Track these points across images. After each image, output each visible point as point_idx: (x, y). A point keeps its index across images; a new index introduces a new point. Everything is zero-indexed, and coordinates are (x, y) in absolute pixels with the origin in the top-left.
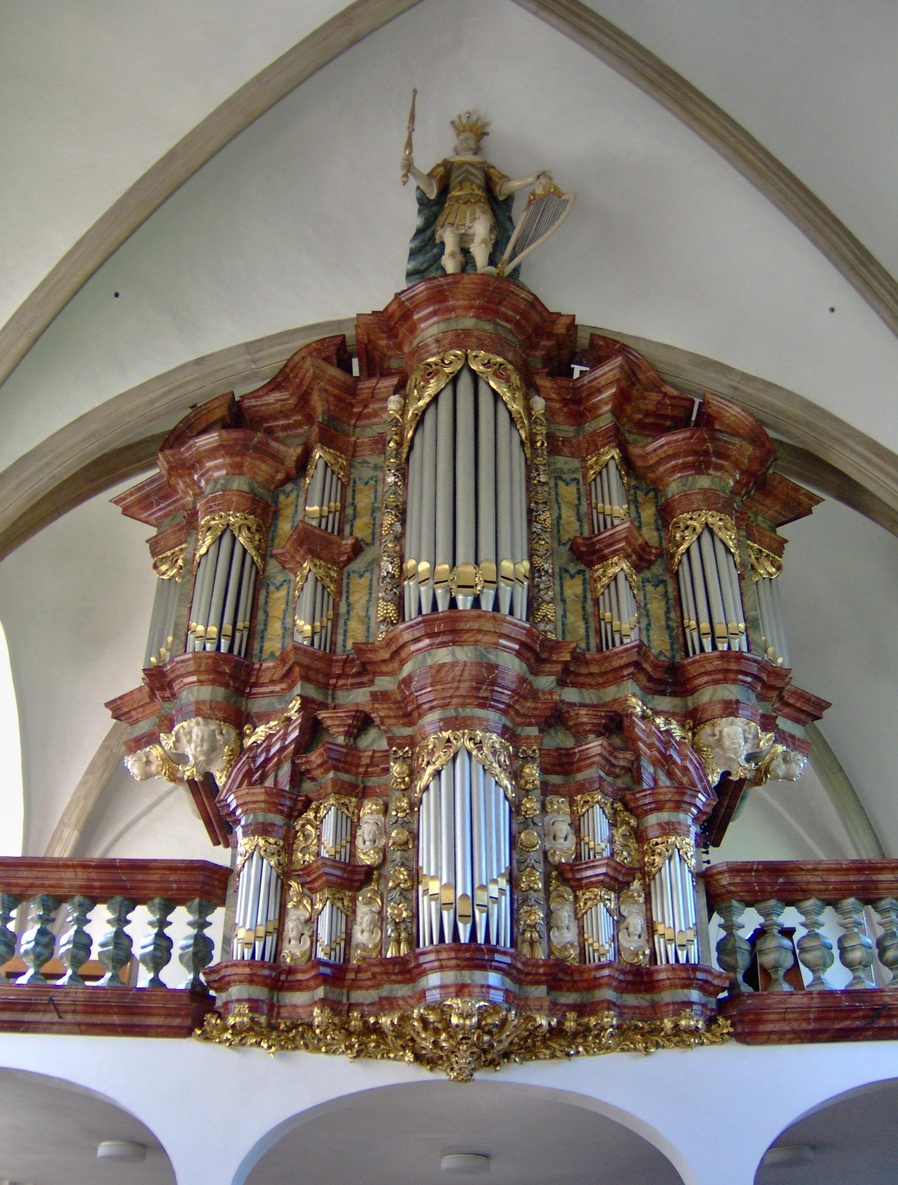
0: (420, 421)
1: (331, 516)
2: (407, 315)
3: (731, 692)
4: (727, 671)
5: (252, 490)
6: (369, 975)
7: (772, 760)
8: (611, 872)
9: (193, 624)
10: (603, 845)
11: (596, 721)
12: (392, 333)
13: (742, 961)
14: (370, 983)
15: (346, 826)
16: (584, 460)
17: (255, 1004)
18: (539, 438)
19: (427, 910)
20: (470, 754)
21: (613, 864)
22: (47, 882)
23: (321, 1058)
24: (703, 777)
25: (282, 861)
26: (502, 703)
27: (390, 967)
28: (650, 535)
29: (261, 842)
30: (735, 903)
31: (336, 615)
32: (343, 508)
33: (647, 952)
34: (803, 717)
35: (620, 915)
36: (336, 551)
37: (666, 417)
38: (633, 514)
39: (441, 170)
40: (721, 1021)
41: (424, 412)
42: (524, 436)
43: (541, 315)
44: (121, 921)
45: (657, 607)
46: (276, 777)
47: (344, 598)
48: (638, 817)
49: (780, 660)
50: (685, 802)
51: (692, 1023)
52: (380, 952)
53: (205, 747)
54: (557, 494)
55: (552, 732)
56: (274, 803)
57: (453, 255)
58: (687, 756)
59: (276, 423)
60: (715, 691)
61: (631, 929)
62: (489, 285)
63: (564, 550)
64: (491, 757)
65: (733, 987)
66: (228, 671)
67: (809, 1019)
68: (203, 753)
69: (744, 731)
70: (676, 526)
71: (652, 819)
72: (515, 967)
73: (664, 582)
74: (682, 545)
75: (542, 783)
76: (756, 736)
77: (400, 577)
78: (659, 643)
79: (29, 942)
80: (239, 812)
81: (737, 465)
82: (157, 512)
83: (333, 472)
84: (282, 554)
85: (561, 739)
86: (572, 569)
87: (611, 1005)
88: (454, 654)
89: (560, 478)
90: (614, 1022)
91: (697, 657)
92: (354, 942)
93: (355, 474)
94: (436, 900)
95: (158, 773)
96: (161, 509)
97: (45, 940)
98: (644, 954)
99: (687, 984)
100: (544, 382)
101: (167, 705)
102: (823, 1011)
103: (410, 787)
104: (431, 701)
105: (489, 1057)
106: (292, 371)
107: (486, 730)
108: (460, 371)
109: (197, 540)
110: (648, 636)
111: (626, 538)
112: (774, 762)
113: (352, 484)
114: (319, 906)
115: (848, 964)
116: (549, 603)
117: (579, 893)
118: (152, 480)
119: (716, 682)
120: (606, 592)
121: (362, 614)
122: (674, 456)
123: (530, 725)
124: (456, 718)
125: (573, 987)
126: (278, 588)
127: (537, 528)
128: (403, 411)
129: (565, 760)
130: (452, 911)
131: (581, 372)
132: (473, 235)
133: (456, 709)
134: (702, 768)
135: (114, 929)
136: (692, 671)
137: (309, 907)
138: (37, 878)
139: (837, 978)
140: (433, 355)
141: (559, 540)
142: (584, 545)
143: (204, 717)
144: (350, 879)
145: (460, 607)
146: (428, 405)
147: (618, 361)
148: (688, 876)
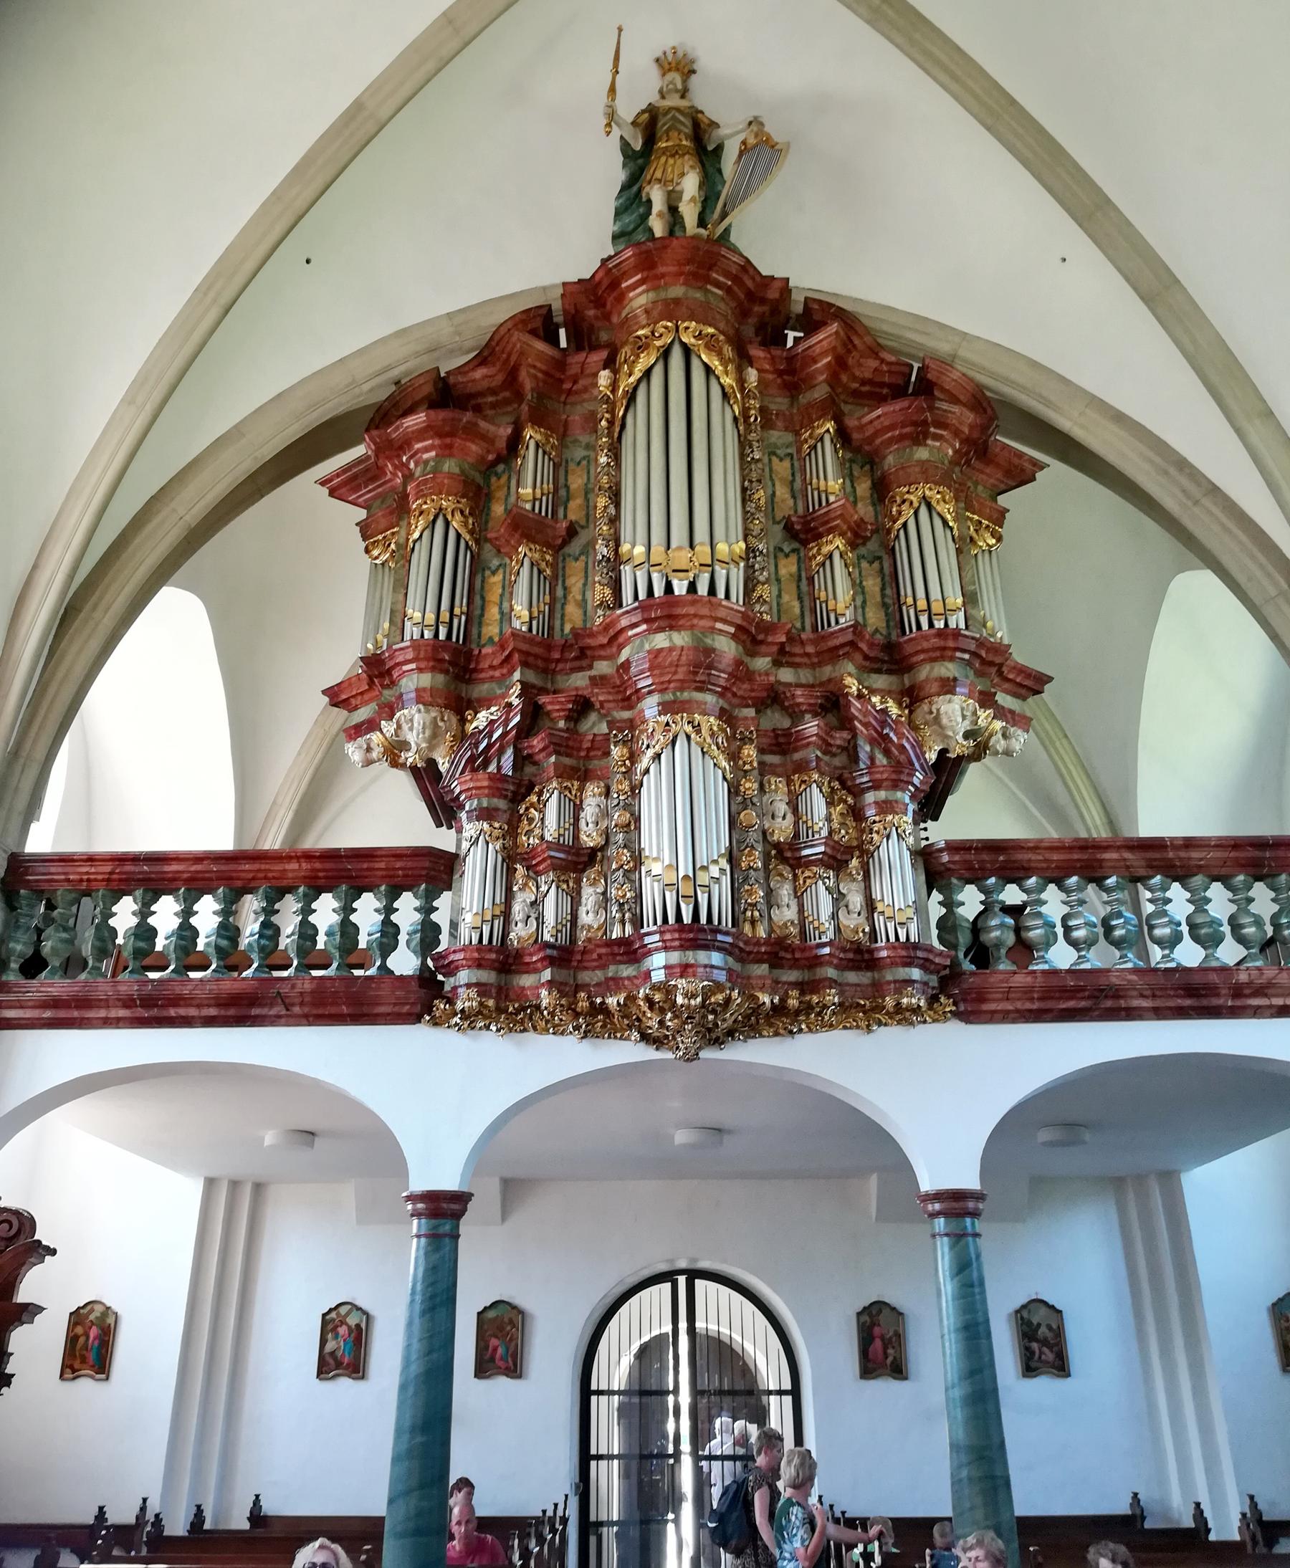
0: (631, 398)
1: (544, 498)
2: (614, 284)
3: (948, 669)
4: (944, 649)
5: (462, 471)
6: (595, 956)
7: (991, 736)
8: (829, 851)
9: (410, 611)
10: (821, 824)
11: (812, 701)
12: (599, 303)
13: (964, 939)
15: (569, 809)
16: (797, 434)
18: (753, 412)
19: (651, 892)
20: (688, 737)
22: (270, 875)
23: (549, 1039)
24: (921, 755)
28: (865, 510)
29: (486, 826)
30: (954, 881)
31: (553, 599)
33: (867, 930)
34: (1023, 691)
36: (555, 536)
37: (882, 385)
38: (849, 489)
41: (635, 389)
44: (347, 910)
45: (872, 584)
46: (499, 762)
47: (560, 582)
48: (855, 796)
51: (914, 1001)
52: (605, 933)
53: (428, 733)
54: (771, 470)
56: (498, 789)
57: (660, 215)
60: (932, 669)
61: (851, 907)
62: (698, 249)
63: (778, 528)
64: (709, 740)
65: (955, 964)
68: (425, 740)
69: (962, 709)
72: (737, 946)
73: (879, 558)
75: (759, 763)
76: (975, 713)
77: (615, 562)
78: (875, 619)
79: (252, 935)
80: (462, 797)
81: (957, 433)
82: (366, 494)
83: (544, 453)
84: (496, 539)
85: (776, 719)
86: (787, 549)
87: (833, 983)
88: (671, 640)
90: (836, 1000)
92: (580, 923)
93: (567, 454)
95: (379, 760)
96: (369, 491)
97: (269, 932)
98: (863, 931)
99: (909, 963)
100: (756, 352)
101: (386, 692)
106: (497, 344)
107: (704, 713)
111: (841, 515)
112: (993, 739)
114: (544, 888)
115: (1074, 943)
116: (763, 584)
117: (799, 872)
118: (359, 461)
121: (579, 597)
122: (892, 427)
123: (747, 706)
124: (674, 702)
125: (795, 964)
126: (494, 573)
127: (751, 507)
128: (614, 386)
129: (781, 740)
131: (795, 338)
132: (681, 192)
133: (674, 694)
134: (920, 746)
136: (909, 649)
137: (534, 889)
138: (259, 871)
139: (1061, 956)
140: (643, 327)
142: (798, 523)
143: (424, 705)
144: (576, 861)
145: (676, 593)
146: (639, 381)
147: (834, 327)
148: (907, 854)
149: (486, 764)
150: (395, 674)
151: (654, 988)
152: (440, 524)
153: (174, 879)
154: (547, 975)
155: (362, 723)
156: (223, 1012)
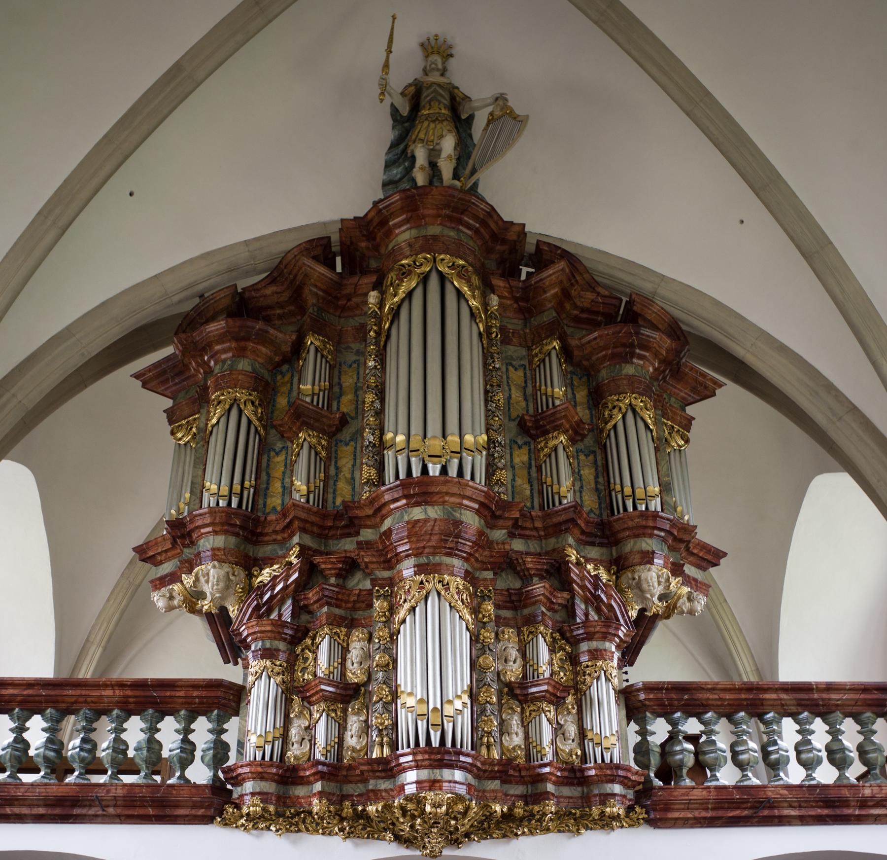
0: (396, 313)
1: (321, 393)
2: (384, 222)
5: (254, 371)
8: (551, 689)
9: (208, 484)
11: (539, 567)
13: (655, 761)
14: (358, 778)
16: (529, 349)
17: (265, 797)
19: (405, 720)
20: (439, 594)
21: (553, 683)
25: (286, 680)
26: (465, 552)
27: (375, 766)
28: (582, 413)
29: (268, 663)
30: (648, 714)
31: (327, 477)
32: (331, 386)
33: (579, 753)
35: (558, 723)
37: (597, 313)
39: (412, 89)
40: (637, 809)
41: (399, 307)
42: (482, 329)
43: (497, 223)
44: (153, 730)
45: (588, 473)
47: (333, 463)
49: (686, 518)
50: (610, 633)
52: (366, 754)
53: (221, 585)
54: (508, 377)
55: (503, 574)
58: (612, 595)
59: (272, 312)
63: (513, 425)
64: (456, 597)
66: (238, 523)
67: (708, 808)
70: (605, 406)
71: (584, 646)
72: (476, 766)
73: (594, 452)
74: (609, 421)
75: (496, 616)
76: (668, 580)
77: (381, 446)
78: (590, 502)
79: (74, 748)
80: (249, 639)
81: (656, 355)
83: (322, 356)
84: (281, 425)
89: (511, 364)
91: (621, 516)
94: (412, 712)
96: (176, 384)
97: (88, 746)
100: (498, 282)
101: (187, 551)
102: (719, 803)
103: (388, 622)
104: (407, 550)
105: (454, 837)
107: (452, 574)
108: (430, 270)
109: (209, 412)
110: (581, 497)
113: (338, 366)
114: (316, 716)
116: (501, 469)
119: (637, 536)
120: (548, 460)
121: (348, 476)
123: (487, 569)
126: (277, 454)
128: (381, 305)
130: (425, 721)
132: (440, 151)
135: (147, 736)
136: (617, 527)
138: (81, 696)
140: (407, 258)
141: (510, 417)
144: (347, 694)
146: (403, 300)
147: (562, 264)
148: (612, 693)
149: (269, 611)
150: (194, 536)
151: (408, 799)
152: (234, 413)
153: (10, 701)
154: (318, 786)
155: (166, 576)
156: (50, 811)
